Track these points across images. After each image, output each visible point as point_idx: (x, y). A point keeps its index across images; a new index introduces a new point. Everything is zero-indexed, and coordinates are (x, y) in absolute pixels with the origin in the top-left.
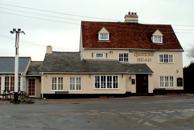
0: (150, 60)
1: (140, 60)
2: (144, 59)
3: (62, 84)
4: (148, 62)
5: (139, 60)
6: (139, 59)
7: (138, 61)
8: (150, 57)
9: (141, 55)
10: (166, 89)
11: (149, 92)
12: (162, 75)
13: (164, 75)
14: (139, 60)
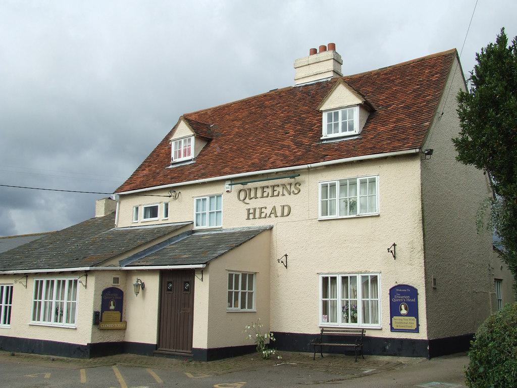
0: (286, 212)
1: (254, 213)
2: (268, 211)
3: (40, 300)
4: (280, 219)
5: (251, 214)
6: (251, 211)
7: (248, 218)
8: (287, 199)
9: (259, 194)
10: (368, 334)
11: (194, 346)
12: (329, 272)
13: (338, 269)
14: (251, 214)
